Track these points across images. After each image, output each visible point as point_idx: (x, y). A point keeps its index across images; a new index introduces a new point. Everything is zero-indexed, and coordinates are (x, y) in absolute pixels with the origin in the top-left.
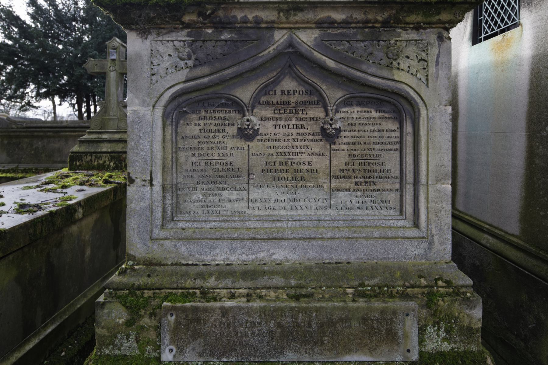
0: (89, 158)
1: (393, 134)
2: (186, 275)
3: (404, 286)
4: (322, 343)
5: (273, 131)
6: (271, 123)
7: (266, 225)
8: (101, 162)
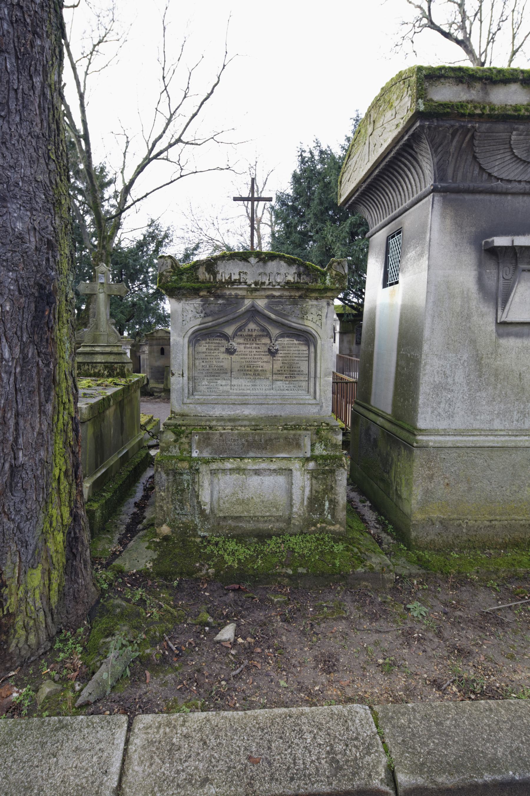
0: (86, 367)
1: (305, 352)
2: (201, 420)
3: (306, 425)
4: (266, 449)
5: (244, 350)
6: (242, 346)
7: (240, 397)
8: (97, 371)
